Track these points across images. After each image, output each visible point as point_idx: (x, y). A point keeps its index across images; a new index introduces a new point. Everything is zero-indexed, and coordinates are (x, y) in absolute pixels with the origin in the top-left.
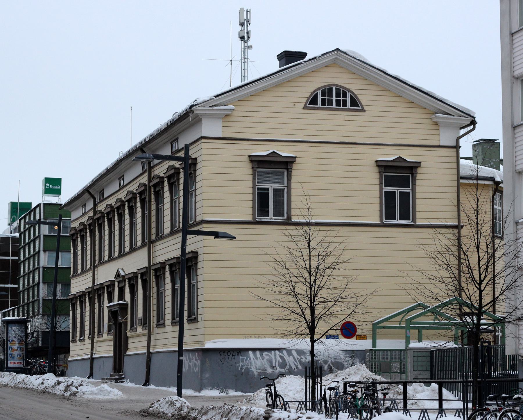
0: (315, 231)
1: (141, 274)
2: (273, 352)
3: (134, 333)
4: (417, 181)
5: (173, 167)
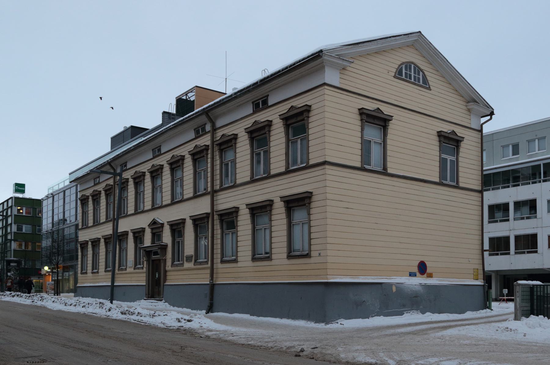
4: (460, 153)
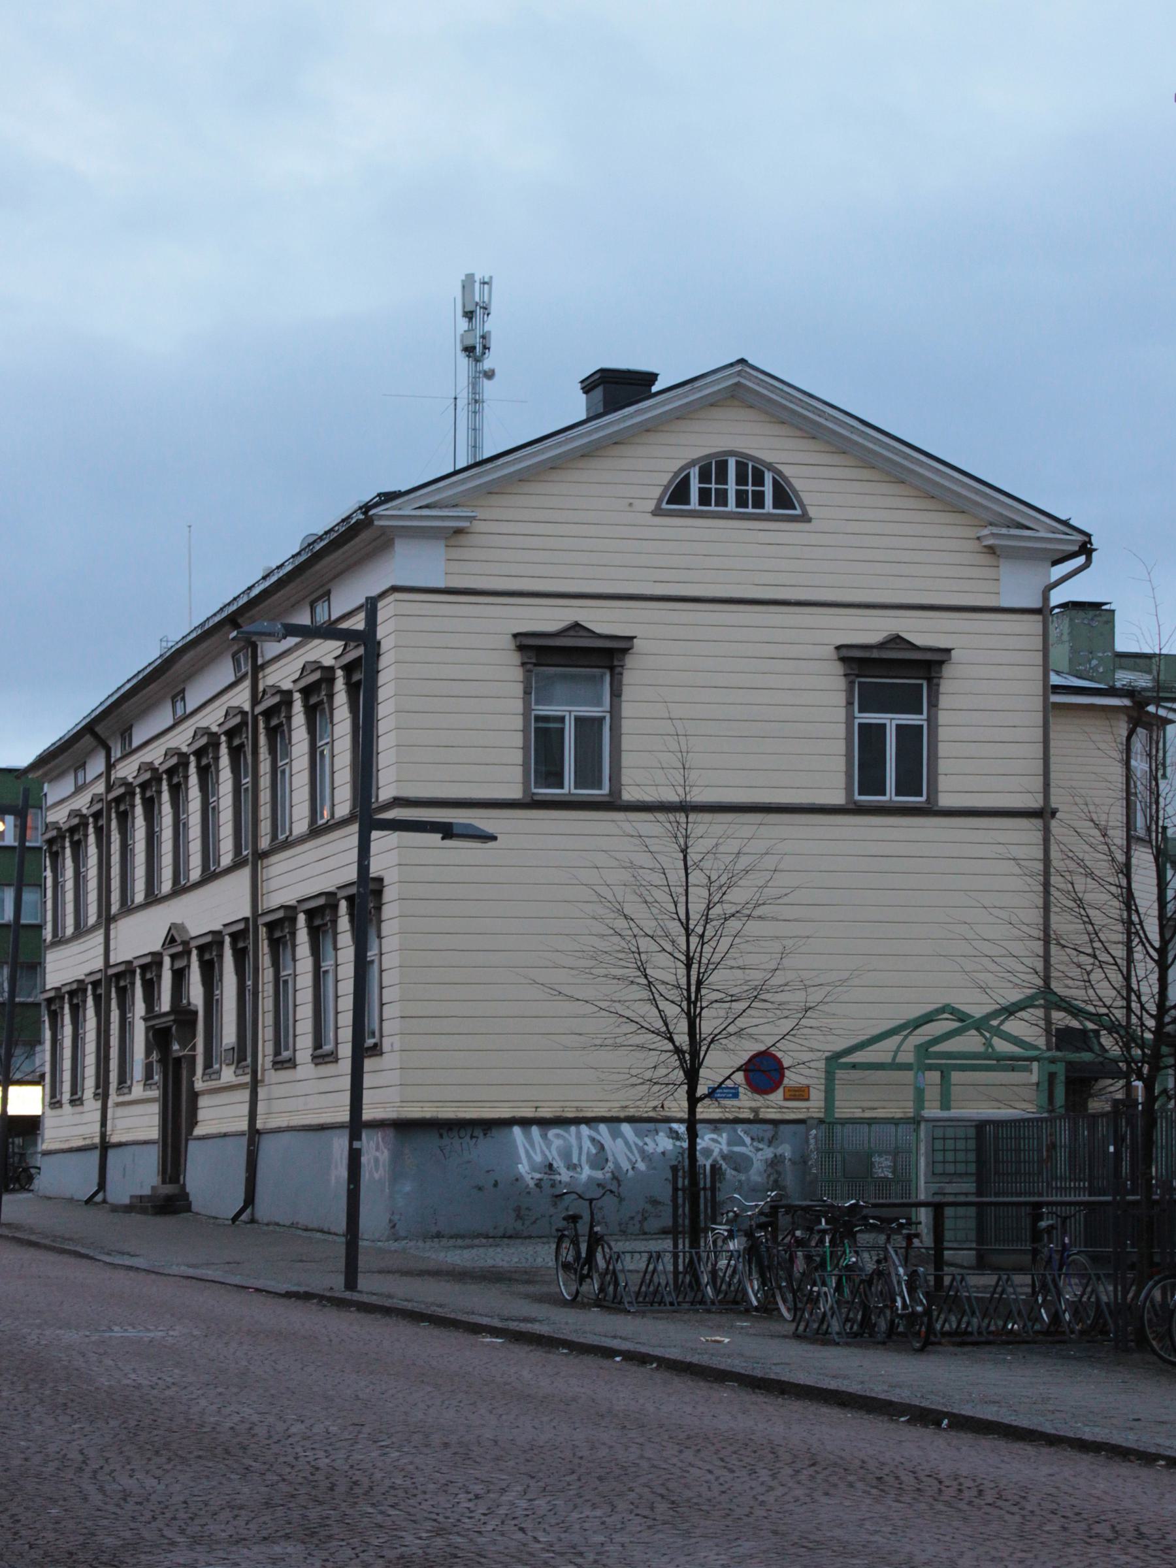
0: (701, 824)
1: (232, 935)
2: (573, 1129)
3: (213, 1083)
5: (205, 731)
